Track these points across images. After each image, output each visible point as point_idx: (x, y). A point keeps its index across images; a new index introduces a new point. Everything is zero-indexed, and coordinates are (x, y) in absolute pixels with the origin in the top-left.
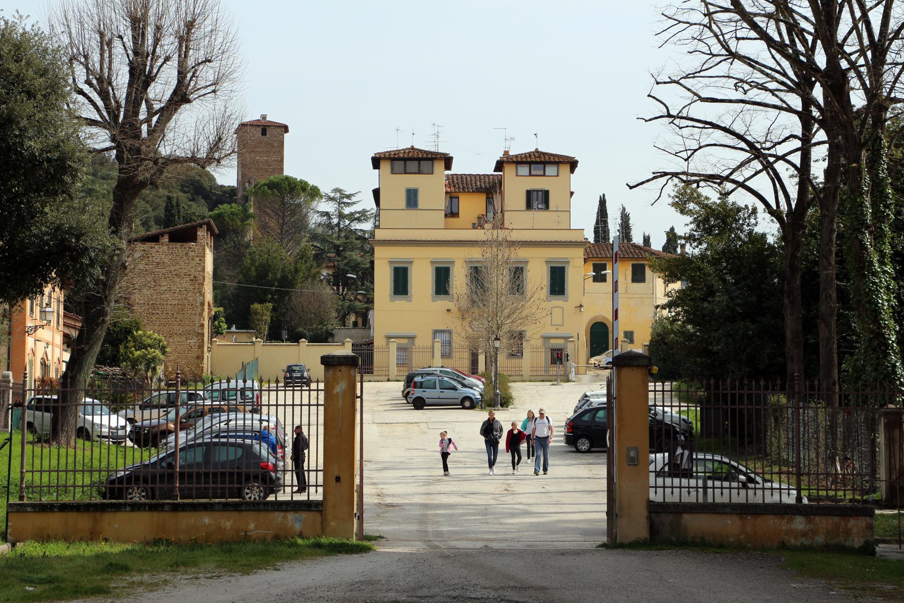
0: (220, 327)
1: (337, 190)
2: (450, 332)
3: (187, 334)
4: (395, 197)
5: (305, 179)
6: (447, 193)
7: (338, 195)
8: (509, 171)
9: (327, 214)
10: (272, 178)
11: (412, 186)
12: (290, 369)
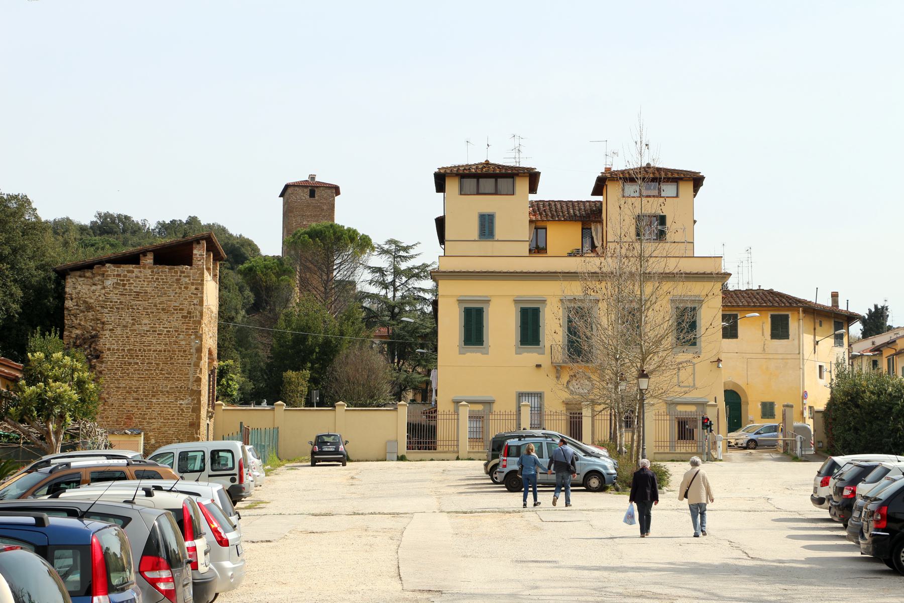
0: (229, 386)
1: (391, 242)
2: (540, 395)
3: (178, 392)
4: (465, 225)
5: (353, 226)
6: (531, 221)
7: (393, 247)
8: (613, 190)
9: (380, 270)
10: (314, 224)
11: (487, 210)
12: (320, 441)
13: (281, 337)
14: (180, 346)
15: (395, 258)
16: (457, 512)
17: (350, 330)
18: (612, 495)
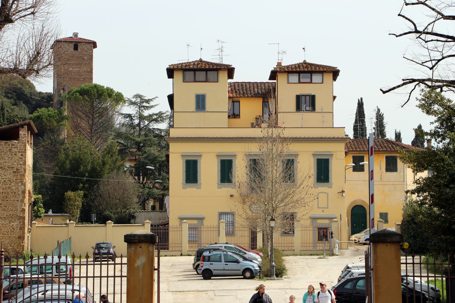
0: (39, 211)
1: (137, 96)
2: (233, 214)
3: (11, 218)
4: (186, 101)
6: (230, 98)
8: (282, 79)
10: (83, 86)
11: (200, 92)
12: (98, 247)
13: (62, 167)
14: (12, 190)
15: (140, 107)
16: (176, 292)
17: (110, 160)
18: (256, 281)
